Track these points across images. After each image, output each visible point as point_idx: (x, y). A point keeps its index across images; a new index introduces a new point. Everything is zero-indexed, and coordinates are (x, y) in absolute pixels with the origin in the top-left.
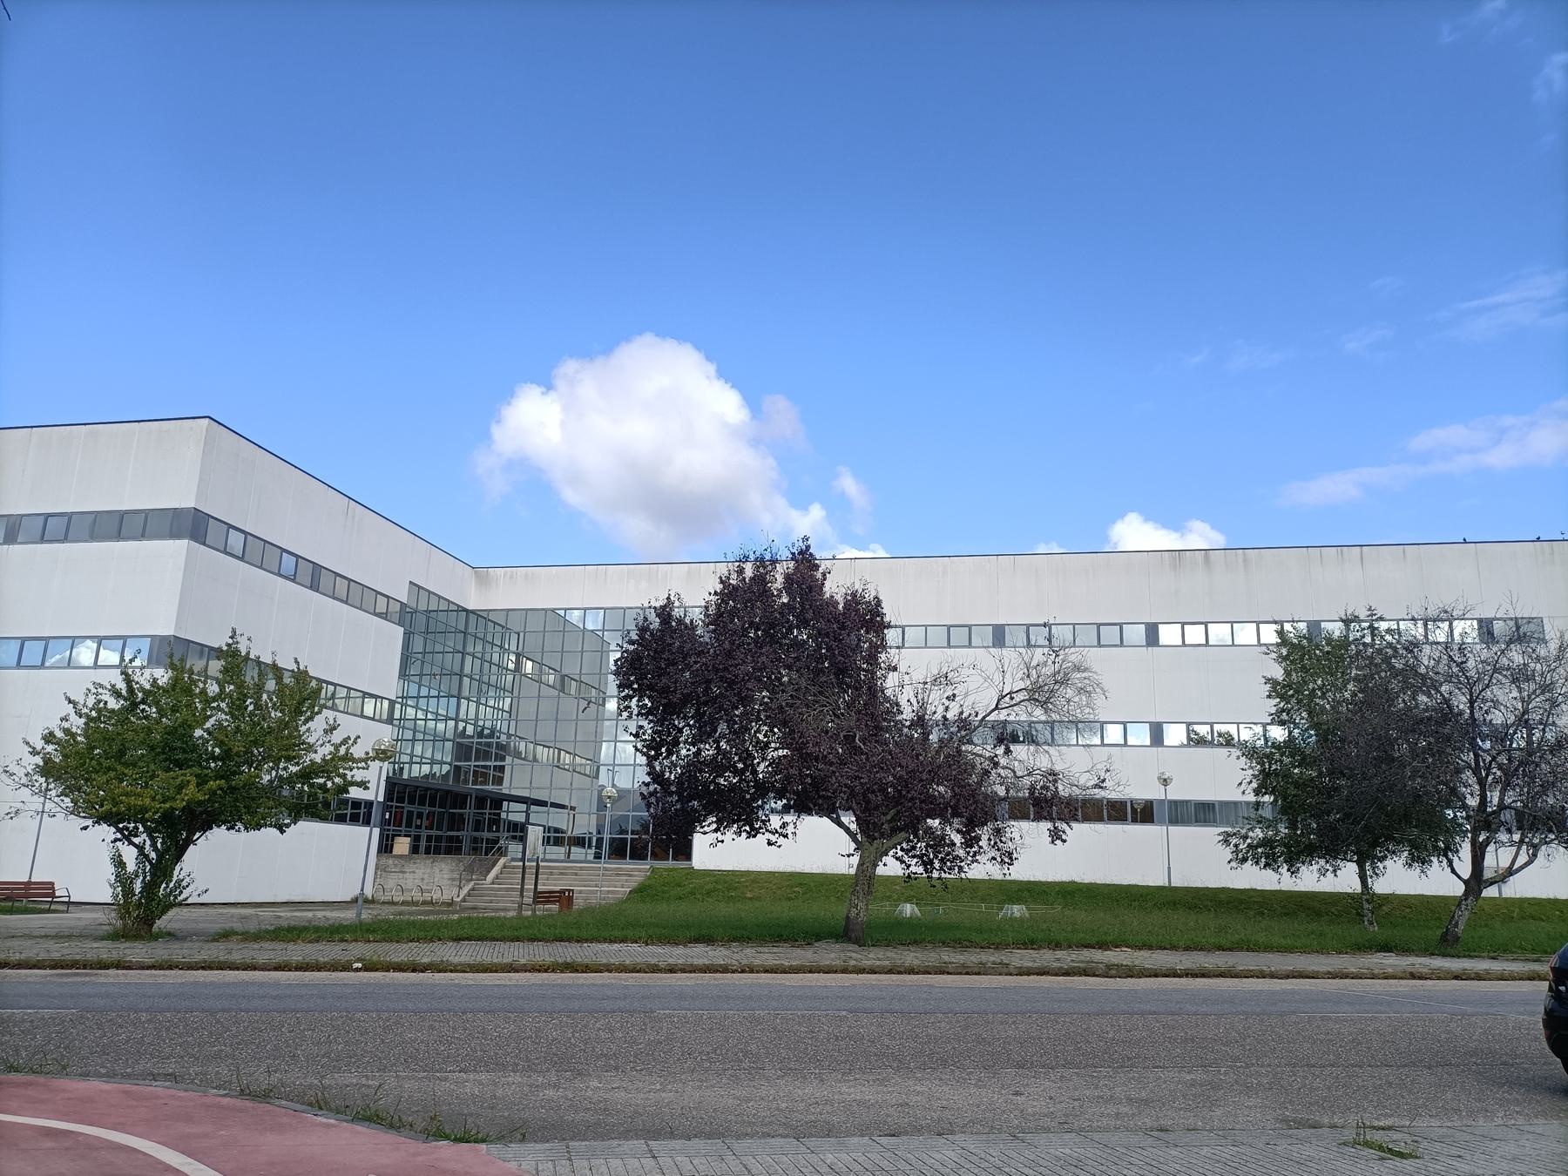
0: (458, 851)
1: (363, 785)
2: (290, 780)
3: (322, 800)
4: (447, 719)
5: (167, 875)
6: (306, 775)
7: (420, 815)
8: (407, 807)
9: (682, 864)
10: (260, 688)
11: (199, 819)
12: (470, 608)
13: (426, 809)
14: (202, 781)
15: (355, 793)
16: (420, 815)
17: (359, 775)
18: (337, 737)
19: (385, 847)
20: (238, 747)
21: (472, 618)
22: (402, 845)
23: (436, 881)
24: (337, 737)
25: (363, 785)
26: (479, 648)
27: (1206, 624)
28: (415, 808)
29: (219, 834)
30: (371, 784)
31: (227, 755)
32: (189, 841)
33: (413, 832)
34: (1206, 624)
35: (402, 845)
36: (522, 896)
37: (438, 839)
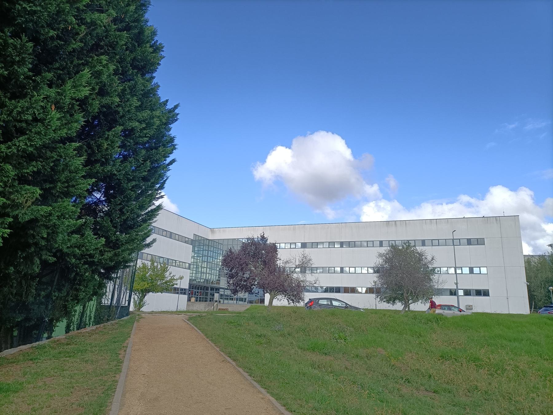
0: (206, 301)
1: (177, 284)
2: (163, 284)
3: (169, 288)
4: (204, 267)
5: (142, 301)
6: (166, 283)
7: (198, 292)
8: (194, 290)
9: (262, 305)
10: (157, 266)
11: (147, 291)
12: (210, 238)
13: (199, 291)
14: (148, 284)
15: (175, 286)
16: (198, 292)
17: (176, 282)
18: (172, 275)
19: (189, 300)
20: (154, 277)
21: (210, 242)
22: (193, 299)
23: (201, 307)
24: (172, 275)
25: (177, 284)
26: (212, 249)
27: (480, 267)
28: (197, 291)
29: (151, 293)
30: (184, 284)
31: (152, 279)
32: (146, 295)
33: (196, 296)
34: (480, 267)
35: (193, 299)
36: (127, 374)
37: (203, 298)
